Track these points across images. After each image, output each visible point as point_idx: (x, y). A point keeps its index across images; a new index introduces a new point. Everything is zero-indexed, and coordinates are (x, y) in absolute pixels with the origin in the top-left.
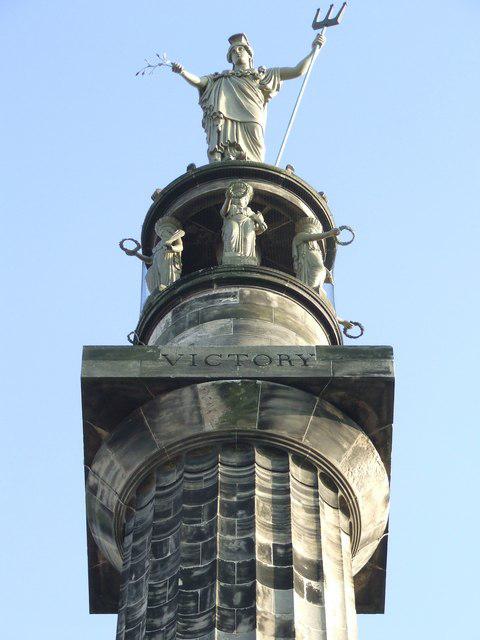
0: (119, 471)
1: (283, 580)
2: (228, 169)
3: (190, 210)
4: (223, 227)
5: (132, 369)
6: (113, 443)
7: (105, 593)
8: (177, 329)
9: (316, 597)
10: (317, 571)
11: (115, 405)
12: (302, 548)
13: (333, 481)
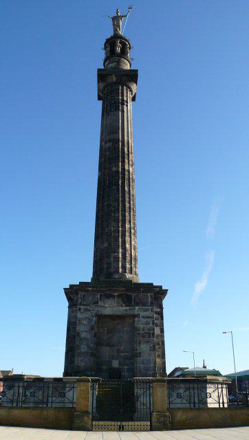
0: (102, 85)
1: (123, 104)
2: (116, 36)
3: (111, 43)
4: (116, 47)
5: (104, 72)
6: (102, 81)
7: (99, 98)
8: (109, 63)
9: (127, 106)
10: (127, 103)
11: (102, 76)
12: (125, 99)
13: (130, 88)
